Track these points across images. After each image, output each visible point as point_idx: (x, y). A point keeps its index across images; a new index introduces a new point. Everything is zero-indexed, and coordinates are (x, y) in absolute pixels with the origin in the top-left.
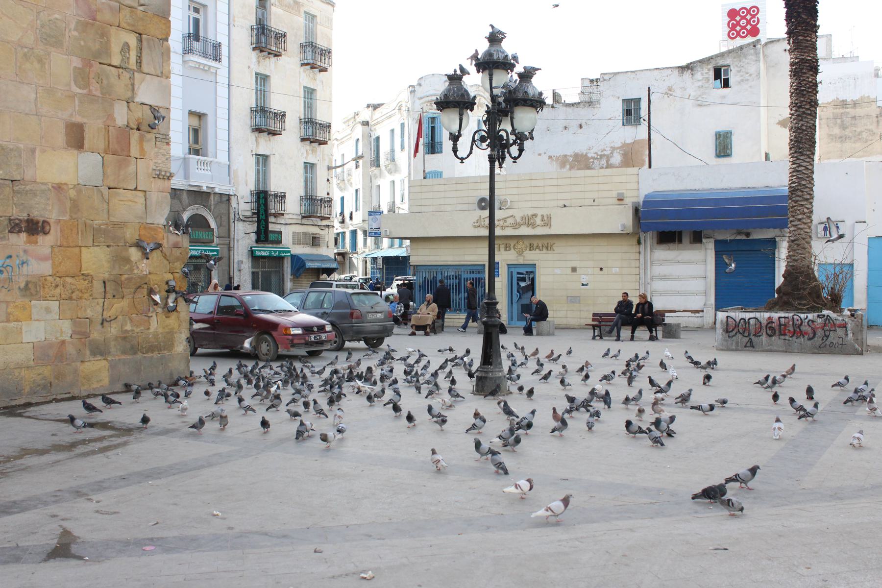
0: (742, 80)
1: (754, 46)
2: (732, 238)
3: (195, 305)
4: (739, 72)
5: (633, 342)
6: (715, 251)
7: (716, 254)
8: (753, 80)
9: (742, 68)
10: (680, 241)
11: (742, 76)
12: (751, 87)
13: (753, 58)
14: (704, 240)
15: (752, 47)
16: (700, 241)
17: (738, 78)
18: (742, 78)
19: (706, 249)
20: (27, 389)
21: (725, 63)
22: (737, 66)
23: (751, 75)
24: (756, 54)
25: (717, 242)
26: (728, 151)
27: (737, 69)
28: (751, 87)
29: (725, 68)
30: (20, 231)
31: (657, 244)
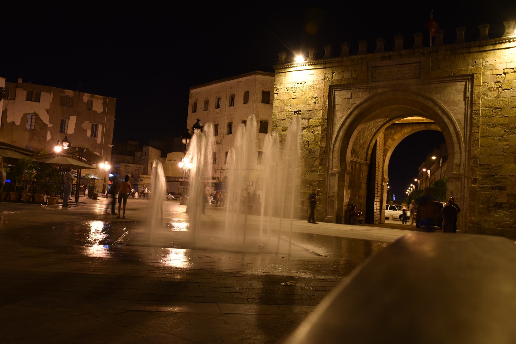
30: (496, 189)
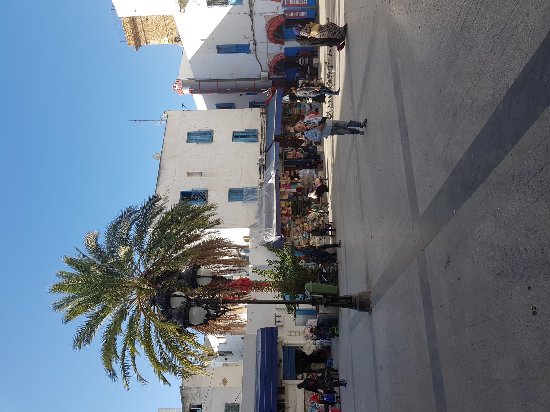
0: (199, 397)
1: (183, 390)
2: (282, 370)
3: (294, 335)
4: (194, 399)
5: (339, 370)
6: (289, 379)
7: (291, 379)
8: (201, 391)
9: (193, 397)
10: (283, 401)
11: (197, 397)
12: (204, 392)
13: (189, 390)
14: (283, 385)
15: (183, 391)
16: (284, 388)
17: (198, 399)
18: (198, 397)
19: (288, 385)
20: (294, 27)
21: (189, 406)
22: (191, 400)
23: (197, 392)
24: (187, 389)
25: (284, 379)
26: (236, 405)
27: (193, 400)
28: (204, 392)
29: (191, 407)
31: (284, 394)
